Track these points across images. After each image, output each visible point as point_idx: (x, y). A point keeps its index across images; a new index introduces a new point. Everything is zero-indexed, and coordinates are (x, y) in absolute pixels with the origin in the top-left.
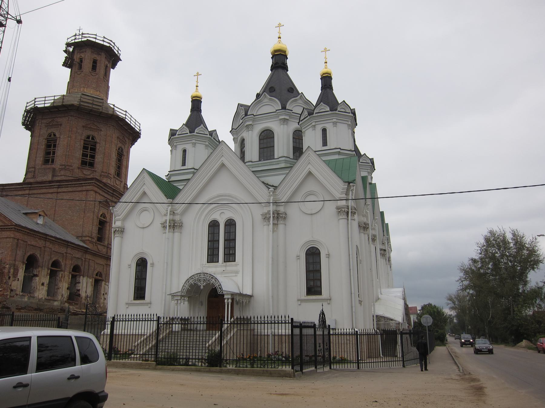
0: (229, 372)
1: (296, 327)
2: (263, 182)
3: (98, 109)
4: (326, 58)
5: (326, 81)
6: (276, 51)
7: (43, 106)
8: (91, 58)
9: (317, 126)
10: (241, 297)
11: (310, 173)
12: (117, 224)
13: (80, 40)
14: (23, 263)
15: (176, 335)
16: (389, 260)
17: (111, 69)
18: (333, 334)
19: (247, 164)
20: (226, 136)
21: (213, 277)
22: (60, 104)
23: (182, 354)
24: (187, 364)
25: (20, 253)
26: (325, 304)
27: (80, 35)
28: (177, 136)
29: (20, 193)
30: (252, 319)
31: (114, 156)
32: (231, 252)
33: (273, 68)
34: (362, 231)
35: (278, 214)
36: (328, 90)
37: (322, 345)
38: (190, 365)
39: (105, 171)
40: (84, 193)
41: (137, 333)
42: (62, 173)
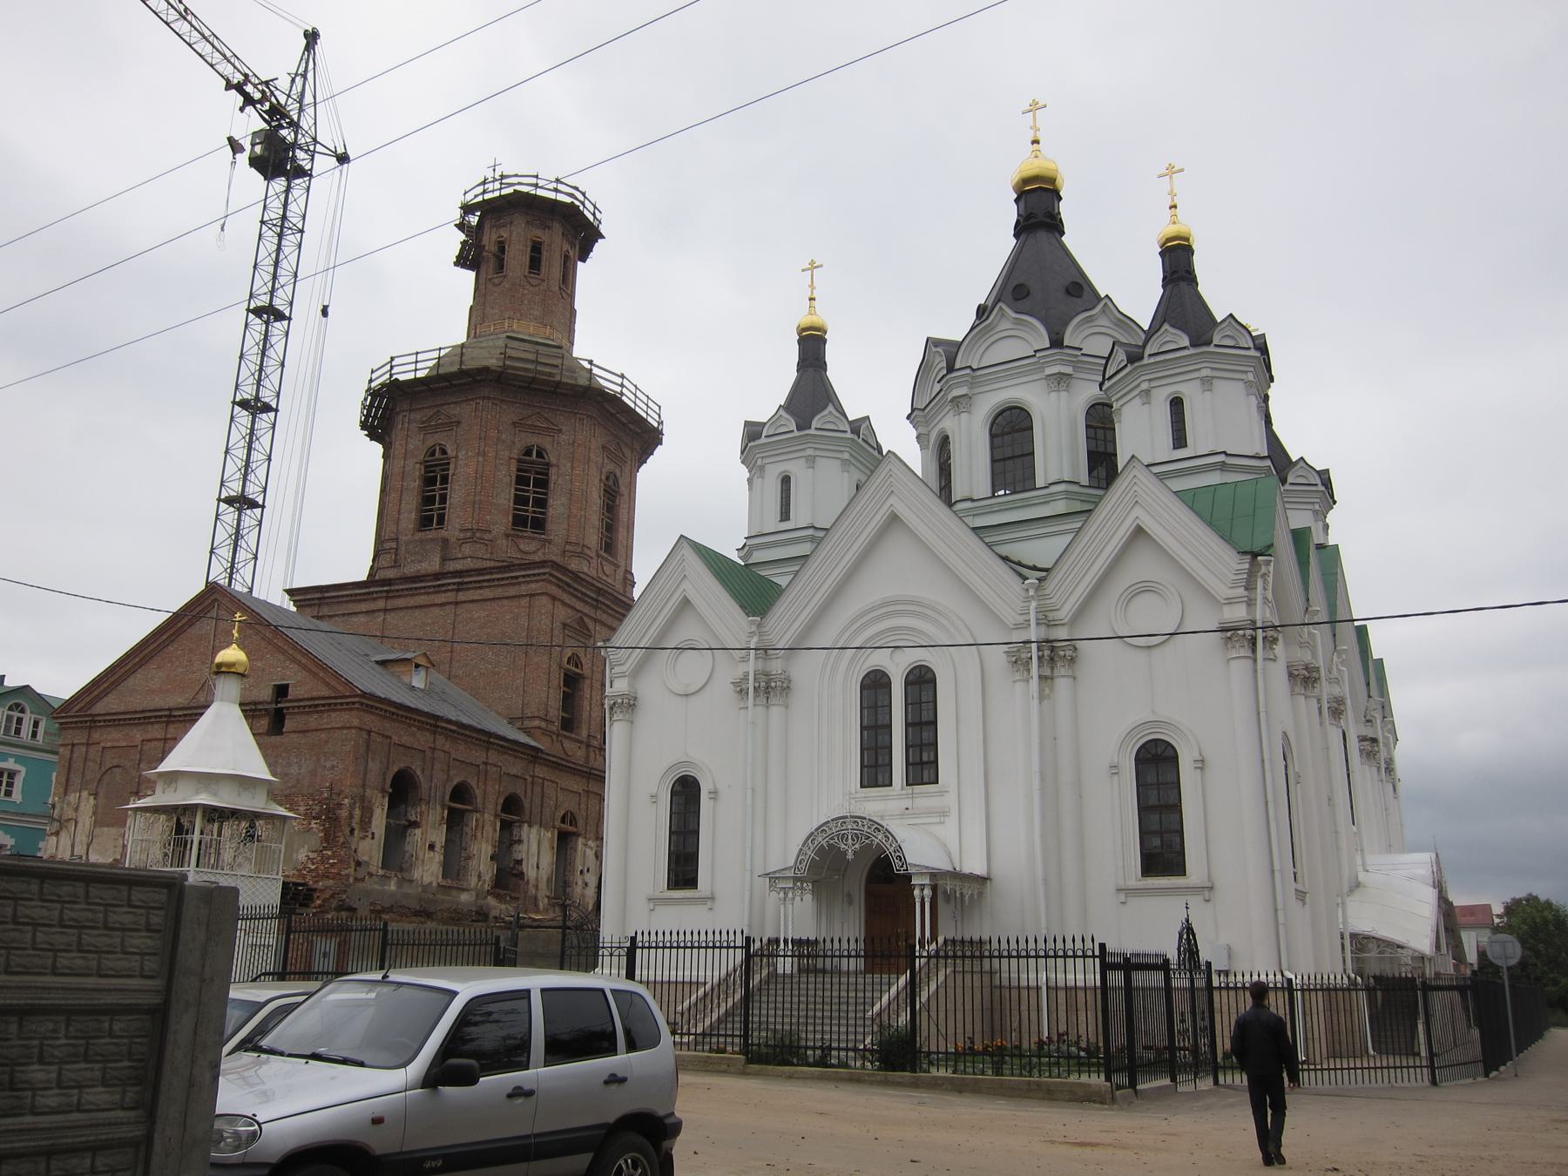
0: (935, 1085)
1: (1115, 967)
2: (1005, 559)
3: (550, 374)
4: (1172, 194)
5: (1177, 260)
6: (1026, 181)
7: (411, 376)
8: (527, 240)
9: (1154, 392)
10: (958, 883)
11: (1139, 532)
12: (618, 686)
13: (497, 194)
14: (383, 791)
15: (788, 986)
16: (1390, 769)
17: (580, 264)
18: (1220, 988)
19: (959, 506)
20: (899, 438)
21: (879, 828)
22: (455, 368)
23: (811, 1038)
24: (822, 1062)
25: (374, 767)
26: (1195, 901)
27: (495, 180)
28: (763, 440)
29: (363, 607)
30: (995, 945)
31: (596, 498)
32: (925, 758)
33: (1020, 230)
34: (1299, 689)
35: (1053, 649)
36: (1183, 285)
37: (1188, 1017)
38: (832, 1066)
39: (573, 539)
40: (525, 601)
41: (659, 978)
42: (467, 550)
